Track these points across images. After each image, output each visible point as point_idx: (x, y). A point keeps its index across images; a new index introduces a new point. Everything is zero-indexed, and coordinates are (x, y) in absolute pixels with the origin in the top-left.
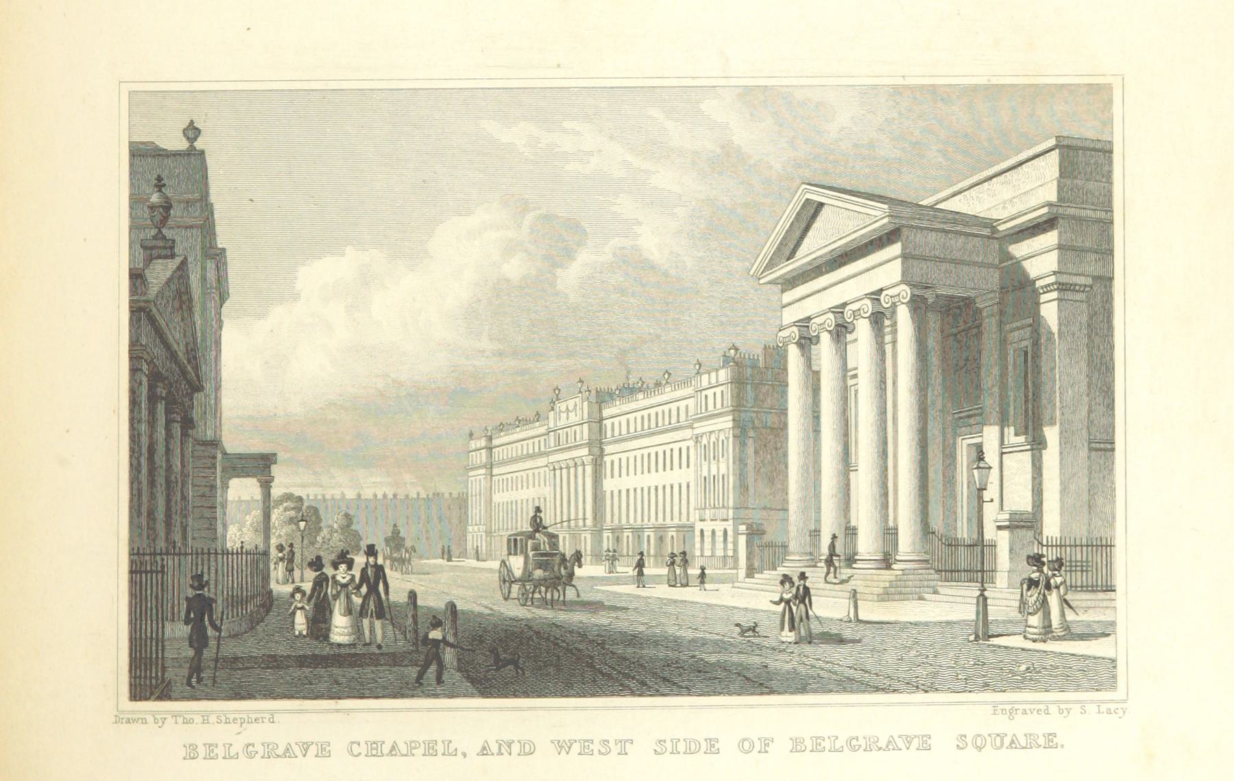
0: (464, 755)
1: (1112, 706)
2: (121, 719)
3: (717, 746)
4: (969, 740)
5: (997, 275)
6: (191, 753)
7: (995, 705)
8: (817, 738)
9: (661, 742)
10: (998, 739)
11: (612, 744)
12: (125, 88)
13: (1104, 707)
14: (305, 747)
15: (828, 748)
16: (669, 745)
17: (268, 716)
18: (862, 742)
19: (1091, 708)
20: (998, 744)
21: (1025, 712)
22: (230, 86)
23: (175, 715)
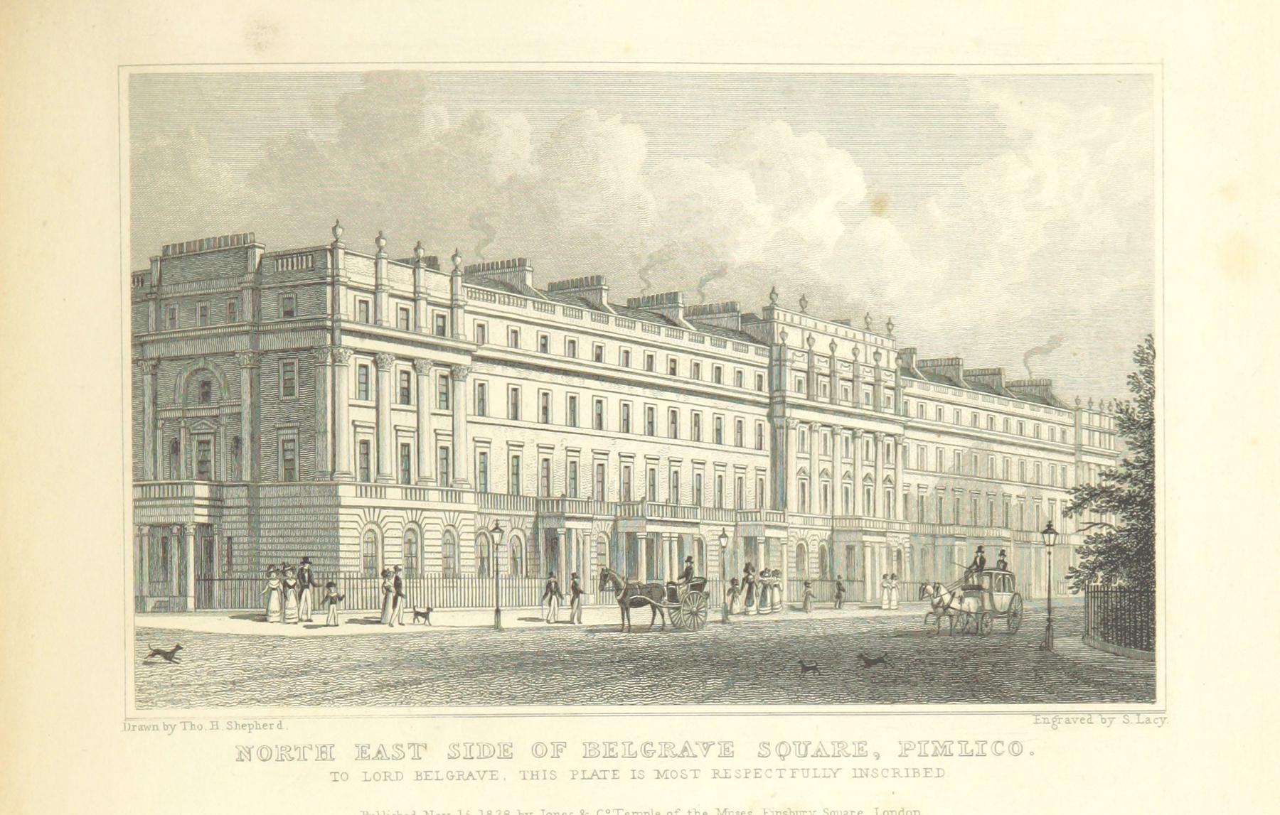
0: (1032, 754)
1: (1152, 717)
2: (129, 725)
3: (511, 750)
4: (772, 748)
5: (529, 282)
6: (244, 754)
7: (1036, 714)
8: (726, 743)
9: (764, 745)
10: (803, 747)
11: (405, 749)
12: (125, 73)
13: (1143, 718)
14: (707, 746)
15: (620, 754)
16: (463, 750)
17: (276, 722)
18: (657, 747)
19: (1096, 718)
20: (803, 752)
21: (1068, 722)
22: (522, 67)
23: (1125, 713)
